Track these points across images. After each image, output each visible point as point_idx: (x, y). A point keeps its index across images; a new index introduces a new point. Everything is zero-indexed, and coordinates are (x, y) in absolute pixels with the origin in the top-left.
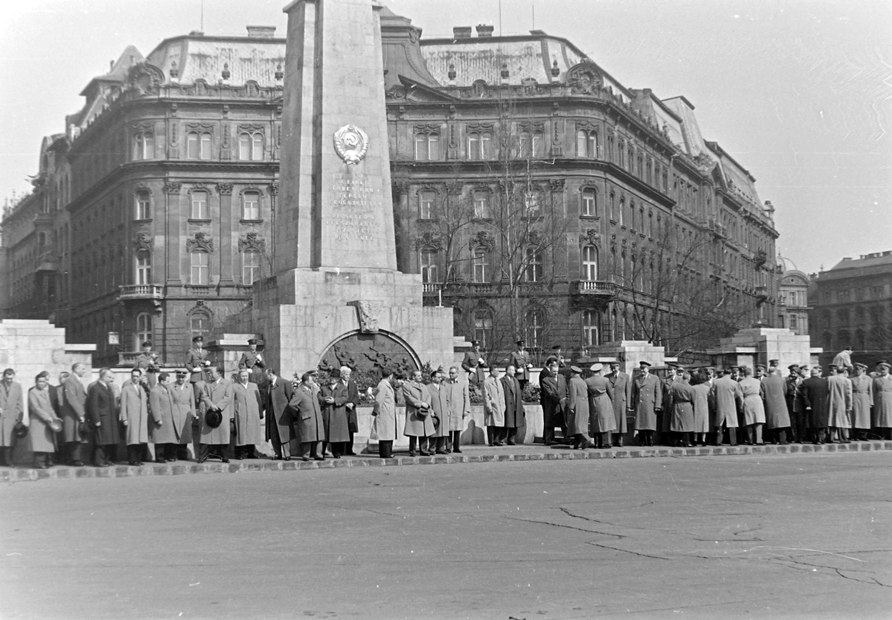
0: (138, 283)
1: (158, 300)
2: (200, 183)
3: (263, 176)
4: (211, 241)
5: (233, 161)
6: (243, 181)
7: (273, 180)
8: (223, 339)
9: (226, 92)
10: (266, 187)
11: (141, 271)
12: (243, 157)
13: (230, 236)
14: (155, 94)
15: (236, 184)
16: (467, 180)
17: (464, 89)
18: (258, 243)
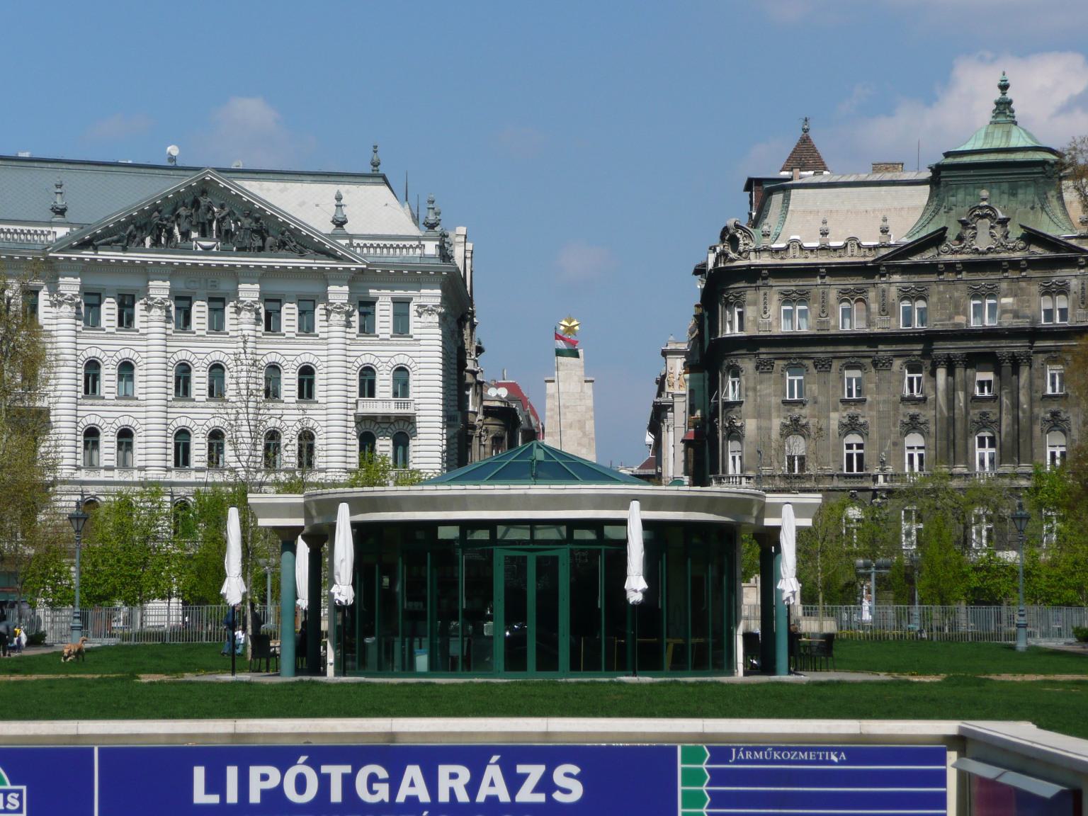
0: (731, 472)
2: (1055, 351)
3: (865, 348)
4: (807, 424)
5: (833, 332)
6: (842, 354)
7: (877, 352)
9: (766, 255)
10: (869, 360)
11: (734, 458)
12: (974, 324)
13: (828, 417)
14: (745, 258)
16: (893, 353)
18: (803, 426)
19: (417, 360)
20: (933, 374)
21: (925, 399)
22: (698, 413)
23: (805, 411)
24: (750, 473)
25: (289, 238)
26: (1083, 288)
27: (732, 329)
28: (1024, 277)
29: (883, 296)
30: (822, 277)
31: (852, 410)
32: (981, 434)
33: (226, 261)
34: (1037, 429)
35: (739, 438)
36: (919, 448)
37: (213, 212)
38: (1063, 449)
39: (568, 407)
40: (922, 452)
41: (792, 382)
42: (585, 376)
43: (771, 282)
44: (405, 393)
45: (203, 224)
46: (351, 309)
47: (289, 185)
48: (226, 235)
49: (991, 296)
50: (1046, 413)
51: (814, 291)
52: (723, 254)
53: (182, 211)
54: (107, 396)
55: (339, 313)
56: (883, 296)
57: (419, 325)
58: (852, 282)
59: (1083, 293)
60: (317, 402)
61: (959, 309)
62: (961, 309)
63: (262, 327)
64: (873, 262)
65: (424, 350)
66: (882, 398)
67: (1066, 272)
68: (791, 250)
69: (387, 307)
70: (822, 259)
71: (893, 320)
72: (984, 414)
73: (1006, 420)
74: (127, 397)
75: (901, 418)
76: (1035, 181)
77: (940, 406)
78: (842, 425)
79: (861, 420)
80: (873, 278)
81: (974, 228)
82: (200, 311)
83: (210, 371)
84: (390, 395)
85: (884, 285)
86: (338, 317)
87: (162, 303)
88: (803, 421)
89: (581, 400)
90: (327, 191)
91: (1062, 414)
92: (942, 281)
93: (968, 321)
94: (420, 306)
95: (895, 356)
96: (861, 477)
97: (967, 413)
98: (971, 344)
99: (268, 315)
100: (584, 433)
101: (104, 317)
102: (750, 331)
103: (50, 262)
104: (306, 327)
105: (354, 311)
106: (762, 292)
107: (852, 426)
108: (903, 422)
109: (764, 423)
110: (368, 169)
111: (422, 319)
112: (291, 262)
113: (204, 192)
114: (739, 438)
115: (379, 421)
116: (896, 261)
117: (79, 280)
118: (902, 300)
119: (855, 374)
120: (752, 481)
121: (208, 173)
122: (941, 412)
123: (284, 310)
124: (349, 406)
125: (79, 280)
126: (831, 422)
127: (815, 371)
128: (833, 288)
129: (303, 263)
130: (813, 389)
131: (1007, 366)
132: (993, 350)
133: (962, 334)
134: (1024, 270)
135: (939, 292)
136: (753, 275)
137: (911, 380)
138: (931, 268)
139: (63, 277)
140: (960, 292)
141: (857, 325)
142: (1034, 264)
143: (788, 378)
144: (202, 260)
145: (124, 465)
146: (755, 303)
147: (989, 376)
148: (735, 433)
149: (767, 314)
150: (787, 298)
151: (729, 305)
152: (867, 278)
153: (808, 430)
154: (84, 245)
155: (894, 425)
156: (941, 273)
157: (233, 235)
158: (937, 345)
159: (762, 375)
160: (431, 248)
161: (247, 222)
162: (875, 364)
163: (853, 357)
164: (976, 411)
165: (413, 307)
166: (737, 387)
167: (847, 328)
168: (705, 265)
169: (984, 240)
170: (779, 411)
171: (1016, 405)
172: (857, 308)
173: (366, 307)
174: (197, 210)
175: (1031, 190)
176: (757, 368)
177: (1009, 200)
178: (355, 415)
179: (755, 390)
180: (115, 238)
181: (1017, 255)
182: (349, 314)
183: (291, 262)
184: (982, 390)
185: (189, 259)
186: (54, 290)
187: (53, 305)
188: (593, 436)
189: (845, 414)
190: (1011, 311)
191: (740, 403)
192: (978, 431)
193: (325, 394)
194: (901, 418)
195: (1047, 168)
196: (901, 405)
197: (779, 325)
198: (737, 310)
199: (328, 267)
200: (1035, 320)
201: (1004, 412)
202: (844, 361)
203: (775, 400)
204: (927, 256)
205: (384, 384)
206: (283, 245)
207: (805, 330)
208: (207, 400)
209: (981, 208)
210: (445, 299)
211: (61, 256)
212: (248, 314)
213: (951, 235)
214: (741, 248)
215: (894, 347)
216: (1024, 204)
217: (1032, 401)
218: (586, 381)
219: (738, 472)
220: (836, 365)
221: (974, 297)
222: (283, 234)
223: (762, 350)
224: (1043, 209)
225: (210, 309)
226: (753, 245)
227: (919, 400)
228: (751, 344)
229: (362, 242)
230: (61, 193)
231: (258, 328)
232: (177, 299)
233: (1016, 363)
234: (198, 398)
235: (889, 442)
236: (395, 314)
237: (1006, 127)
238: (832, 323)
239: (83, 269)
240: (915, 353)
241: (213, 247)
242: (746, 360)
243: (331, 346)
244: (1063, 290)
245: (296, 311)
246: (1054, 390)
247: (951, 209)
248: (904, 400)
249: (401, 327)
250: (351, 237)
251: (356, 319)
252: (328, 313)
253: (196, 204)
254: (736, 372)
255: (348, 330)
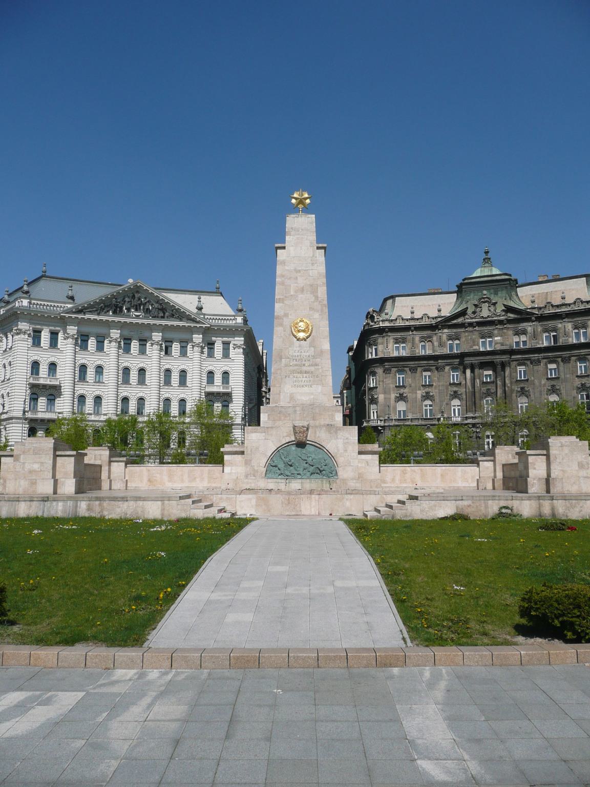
0: (372, 418)
1: (381, 427)
2: (521, 360)
3: (432, 362)
4: (407, 396)
7: (438, 363)
8: (223, 447)
9: (387, 322)
10: (434, 367)
11: (373, 412)
13: (416, 393)
15: (419, 366)
17: (540, 308)
19: (233, 368)
20: (464, 372)
21: (460, 384)
22: (350, 405)
23: (406, 390)
24: (381, 419)
25: (177, 313)
26: (534, 331)
27: (372, 355)
28: (506, 327)
29: (440, 338)
30: (412, 331)
31: (427, 390)
32: (487, 399)
33: (146, 322)
34: (514, 395)
35: (376, 403)
36: (458, 406)
37: (142, 301)
38: (527, 404)
39: (299, 271)
40: (460, 407)
41: (399, 378)
42: (317, 243)
43: (389, 334)
44: (228, 383)
45: (136, 305)
46: (204, 345)
47: (179, 295)
48: (147, 311)
49: (490, 337)
50: (518, 388)
51: (409, 337)
52: (368, 324)
53: (127, 299)
54: (89, 381)
55: (198, 347)
56: (440, 338)
57: (234, 353)
58: (425, 333)
59: (534, 333)
60: (187, 386)
61: (475, 343)
62: (476, 343)
63: (163, 353)
64: (435, 324)
65: (236, 365)
66: (440, 384)
67: (525, 324)
68: (398, 320)
69: (220, 345)
70: (412, 323)
71: (445, 349)
72: (489, 389)
73: (500, 392)
74: (99, 382)
75: (450, 392)
76: (506, 288)
77: (468, 387)
78: (423, 396)
79: (431, 394)
80: (435, 331)
81: (481, 307)
82: (135, 345)
83: (139, 371)
84: (220, 384)
85: (440, 334)
86: (197, 348)
87: (116, 340)
88: (405, 395)
89: (313, 264)
90: (194, 298)
91: (526, 388)
92: (467, 331)
93: (480, 348)
94: (234, 345)
95: (446, 365)
96: (432, 419)
97: (481, 389)
98: (481, 358)
99: (167, 348)
100: (317, 297)
101: (89, 346)
102: (380, 355)
103: (63, 318)
104: (184, 353)
105: (205, 346)
106: (385, 338)
107: (427, 396)
108: (450, 394)
109: (387, 396)
110: (215, 290)
111: (235, 351)
112: (176, 323)
113: (138, 292)
114: (376, 403)
115: (215, 395)
116: (445, 323)
117: (77, 327)
118: (449, 340)
119: (428, 373)
120: (382, 422)
121: (139, 282)
122: (469, 389)
123: (173, 346)
124: (202, 388)
125: (77, 327)
126: (418, 395)
127: (410, 373)
128: (417, 336)
129: (181, 324)
130: (409, 381)
131: (499, 367)
132: (493, 360)
133: (478, 354)
134: (505, 324)
135: (465, 336)
136: (382, 331)
137: (453, 375)
138: (462, 325)
139: (69, 326)
140: (475, 336)
141: (429, 352)
142: (510, 321)
143: (398, 376)
144: (135, 321)
145: (97, 413)
146: (382, 344)
147: (490, 372)
148: (374, 401)
149: (388, 348)
150: (397, 341)
151: (370, 345)
152: (433, 331)
153: (407, 398)
154: (80, 311)
155: (447, 396)
156: (467, 328)
157: (150, 311)
158: (466, 359)
159: (386, 375)
160: (240, 320)
161: (156, 305)
162: (437, 369)
163: (427, 366)
164: (485, 388)
165: (231, 345)
166: (375, 381)
167: (423, 354)
168: (353, 346)
169: (485, 312)
170: (394, 390)
171: (504, 384)
172: (428, 345)
173: (211, 345)
174: (134, 300)
175: (504, 292)
176: (384, 372)
177: (494, 296)
178: (205, 393)
179: (383, 381)
180: (94, 309)
181: (502, 318)
182: (203, 348)
183: (176, 323)
184: (486, 379)
185: (128, 320)
186: (65, 332)
187: (65, 339)
188: (325, 302)
189: (424, 391)
190: (500, 343)
191: (376, 388)
192: (486, 397)
193: (191, 383)
194: (450, 392)
195: (511, 282)
196: (449, 387)
197: (393, 353)
198: (374, 347)
199: (192, 325)
200: (511, 346)
201: (499, 388)
202: (423, 368)
203: (392, 386)
204: (460, 320)
205: (218, 379)
206: (172, 316)
207: (404, 355)
208: (137, 384)
209: (484, 298)
210: (246, 342)
211: (67, 315)
212: (156, 346)
213: (469, 311)
214: (376, 320)
215: (445, 361)
216: (501, 298)
217: (511, 383)
218: (318, 248)
219: (376, 418)
220: (419, 369)
221: (482, 338)
222: (173, 311)
223: (386, 364)
224: (510, 299)
225: (140, 345)
226: (381, 319)
227: (458, 384)
228: (381, 361)
229: (209, 317)
230: (71, 290)
231: (161, 353)
232: (125, 339)
233: (503, 365)
234: (132, 383)
235: (444, 403)
236: (223, 349)
237: (490, 268)
238: (417, 351)
239: (79, 323)
240: (455, 363)
241: (140, 315)
242: (379, 369)
243: (194, 361)
244: (524, 332)
245: (179, 346)
246: (521, 377)
247: (468, 302)
248: (450, 384)
249: (226, 355)
250: (205, 315)
251: (206, 350)
252: (193, 346)
253: (134, 297)
254: (374, 374)
255: (202, 355)
